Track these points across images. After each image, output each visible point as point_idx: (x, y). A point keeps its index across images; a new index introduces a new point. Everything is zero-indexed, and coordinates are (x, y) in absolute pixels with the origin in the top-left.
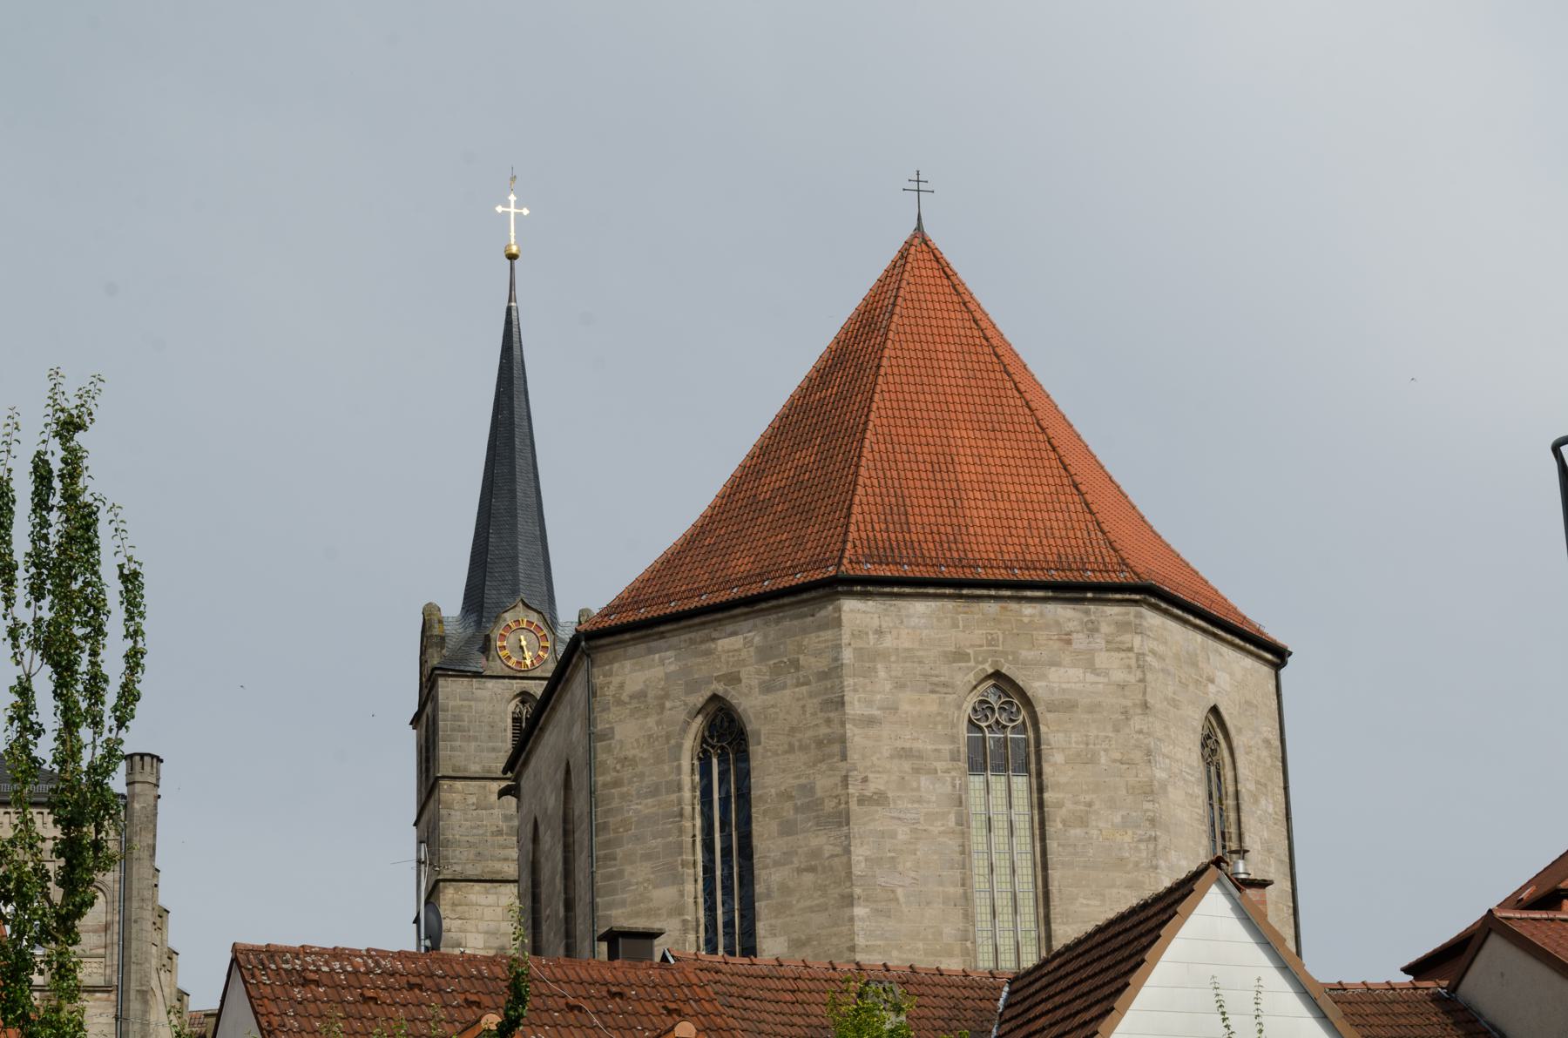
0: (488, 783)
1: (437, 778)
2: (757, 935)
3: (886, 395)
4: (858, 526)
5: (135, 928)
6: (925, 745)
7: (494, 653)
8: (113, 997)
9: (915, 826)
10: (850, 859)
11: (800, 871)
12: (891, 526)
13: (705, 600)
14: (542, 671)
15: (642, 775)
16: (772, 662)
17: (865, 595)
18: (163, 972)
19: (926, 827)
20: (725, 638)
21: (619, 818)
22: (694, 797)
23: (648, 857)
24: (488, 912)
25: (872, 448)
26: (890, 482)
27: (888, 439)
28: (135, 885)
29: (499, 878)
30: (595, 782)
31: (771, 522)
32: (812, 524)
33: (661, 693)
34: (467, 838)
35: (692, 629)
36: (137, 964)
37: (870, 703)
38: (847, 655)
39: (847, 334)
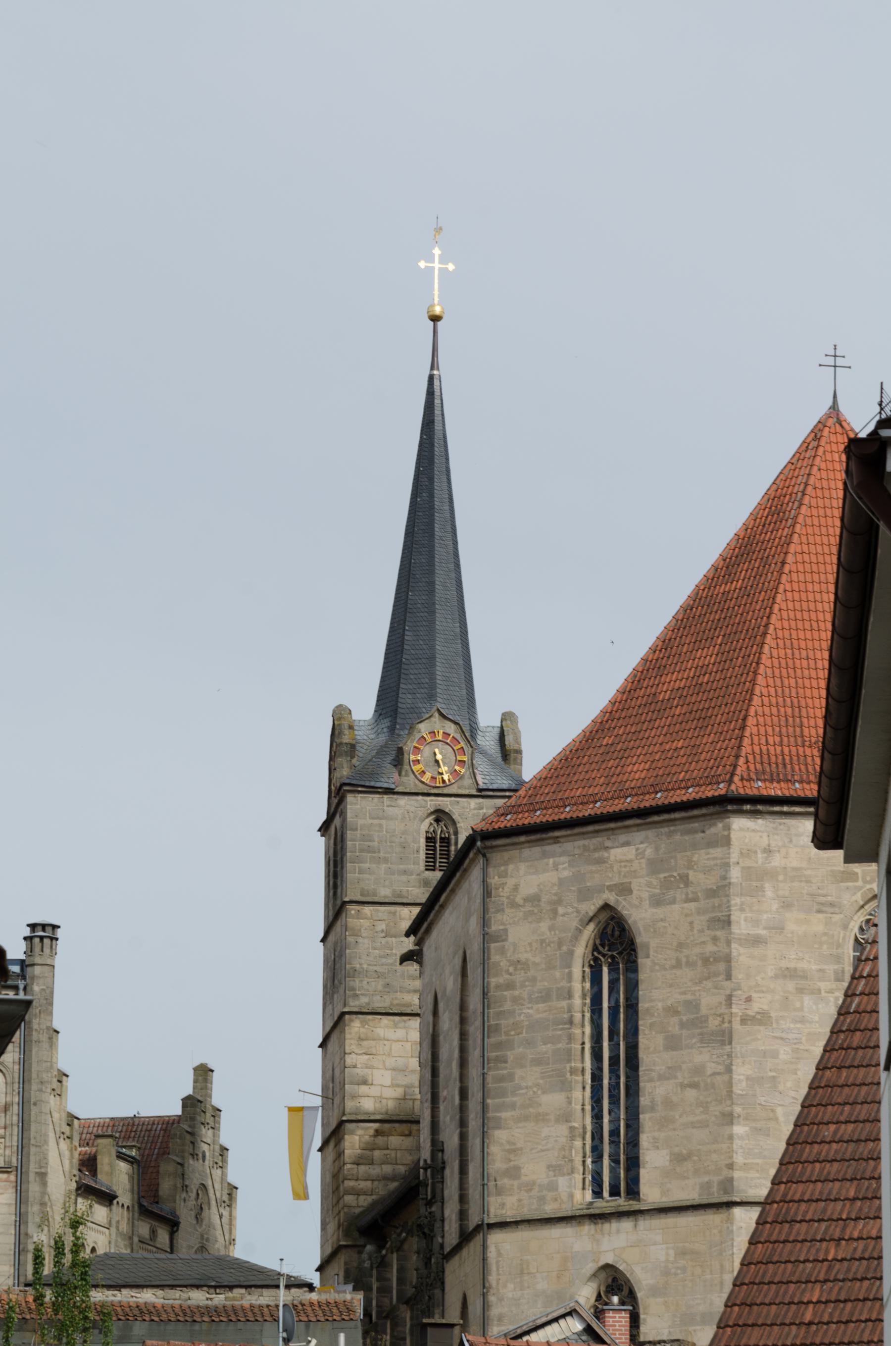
0: (398, 909)
1: (344, 903)
2: (641, 1147)
3: (789, 595)
4: (752, 740)
5: (34, 1111)
6: (810, 965)
7: (407, 767)
8: (12, 1177)
9: (797, 1046)
10: (731, 1078)
11: (683, 1086)
12: (785, 739)
13: (599, 808)
14: (459, 788)
15: (534, 980)
16: (662, 876)
17: (755, 813)
18: (62, 1139)
19: (807, 1048)
20: (617, 847)
21: (511, 1021)
22: (584, 1005)
23: (537, 1062)
24: (396, 1047)
25: (771, 654)
26: (787, 691)
27: (788, 643)
28: (35, 1068)
29: (409, 1012)
30: (488, 983)
31: (669, 726)
32: (707, 733)
33: (555, 898)
34: (375, 968)
35: (586, 836)
36: (36, 1146)
37: (756, 923)
38: (735, 874)
39: (755, 520)
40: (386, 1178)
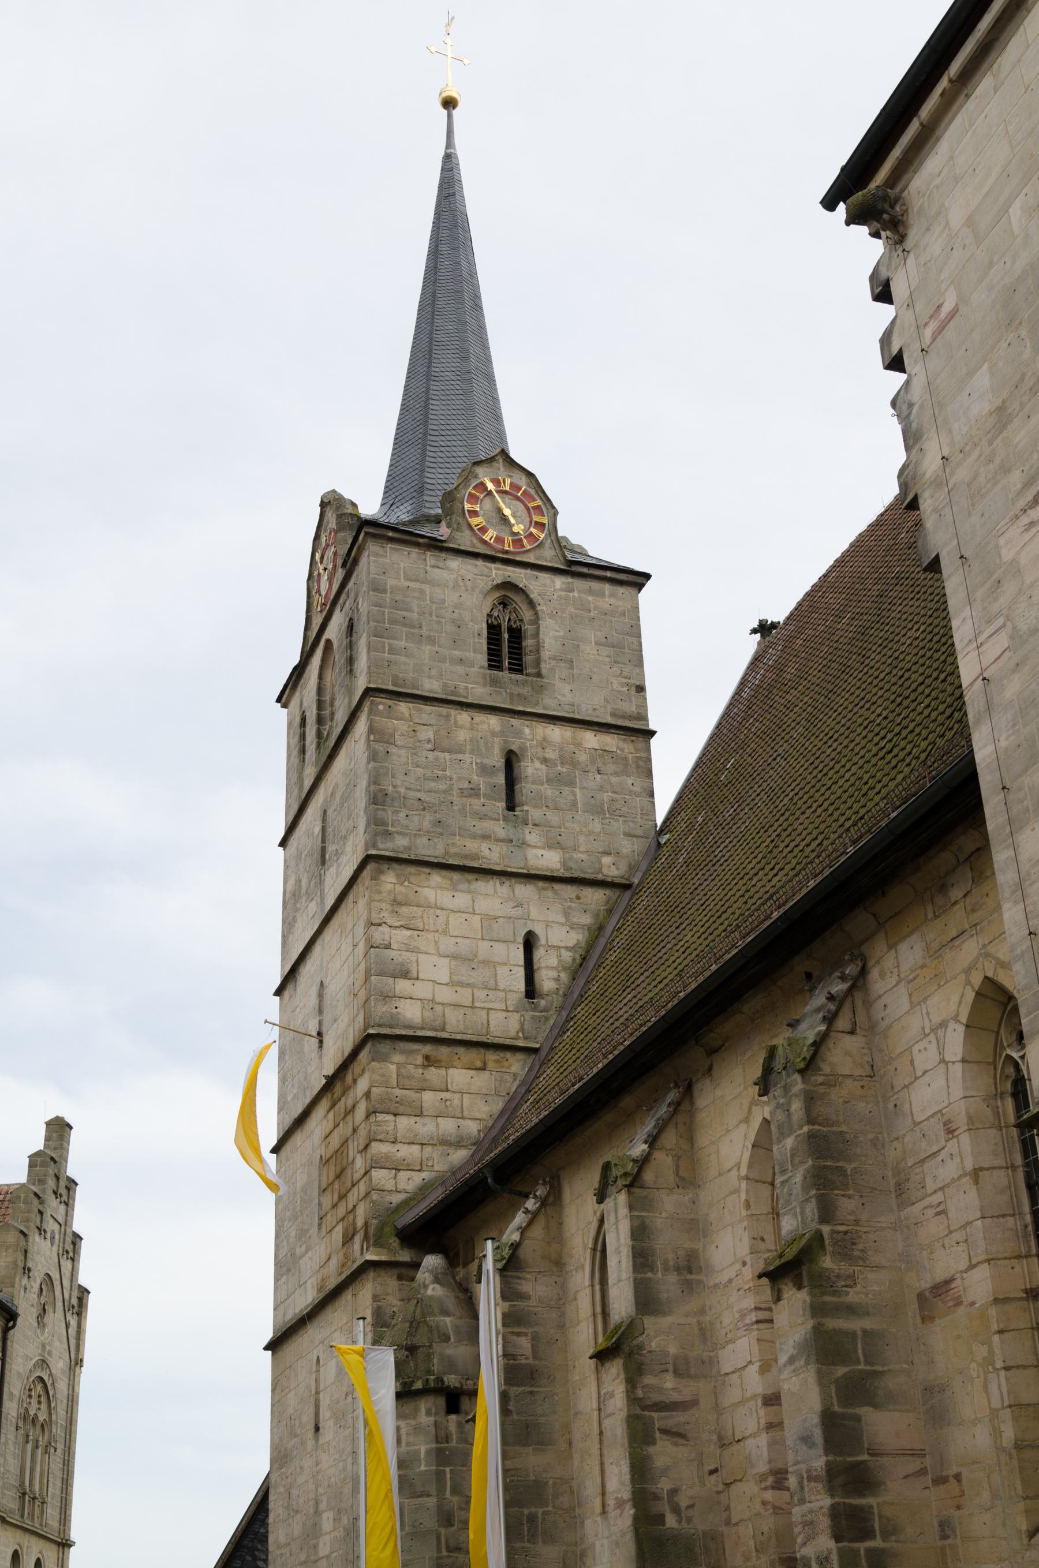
24: (456, 922)
34: (419, 795)
40: (446, 1143)
